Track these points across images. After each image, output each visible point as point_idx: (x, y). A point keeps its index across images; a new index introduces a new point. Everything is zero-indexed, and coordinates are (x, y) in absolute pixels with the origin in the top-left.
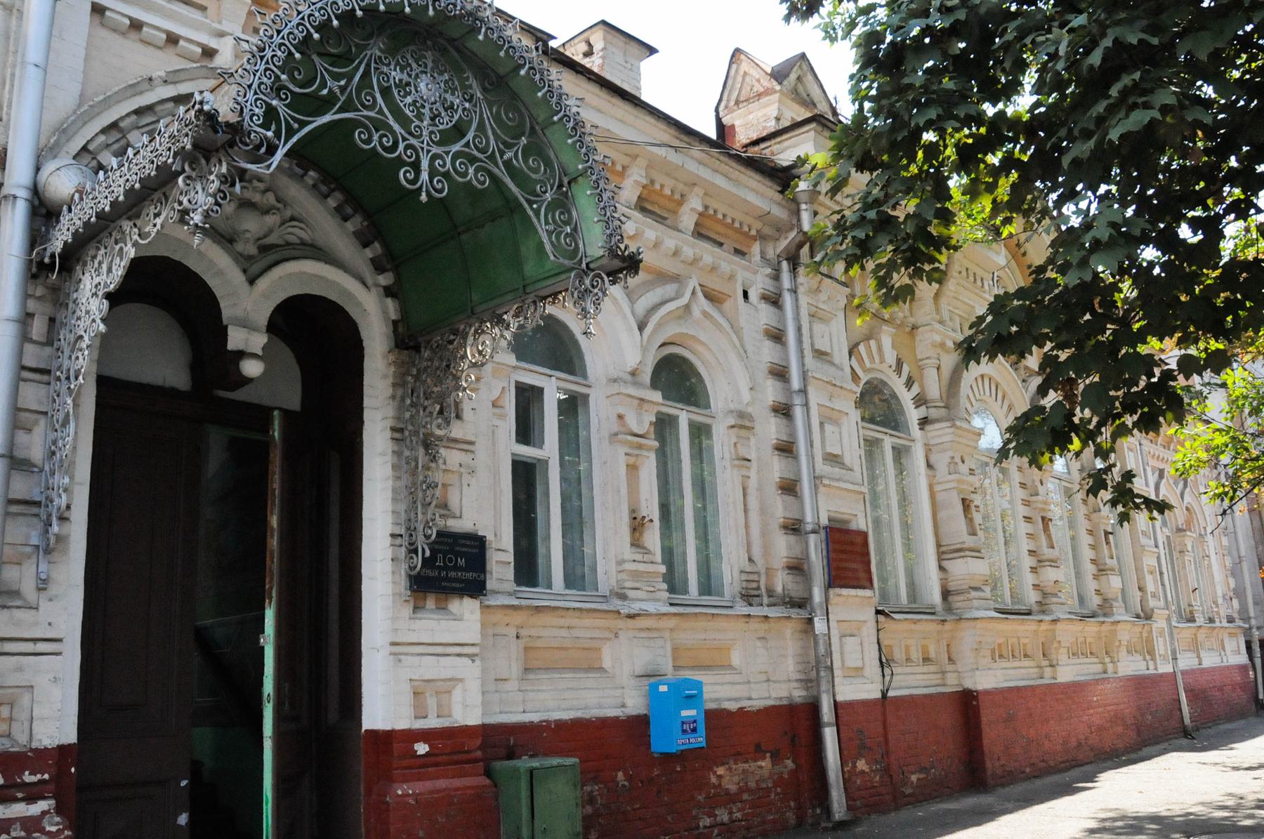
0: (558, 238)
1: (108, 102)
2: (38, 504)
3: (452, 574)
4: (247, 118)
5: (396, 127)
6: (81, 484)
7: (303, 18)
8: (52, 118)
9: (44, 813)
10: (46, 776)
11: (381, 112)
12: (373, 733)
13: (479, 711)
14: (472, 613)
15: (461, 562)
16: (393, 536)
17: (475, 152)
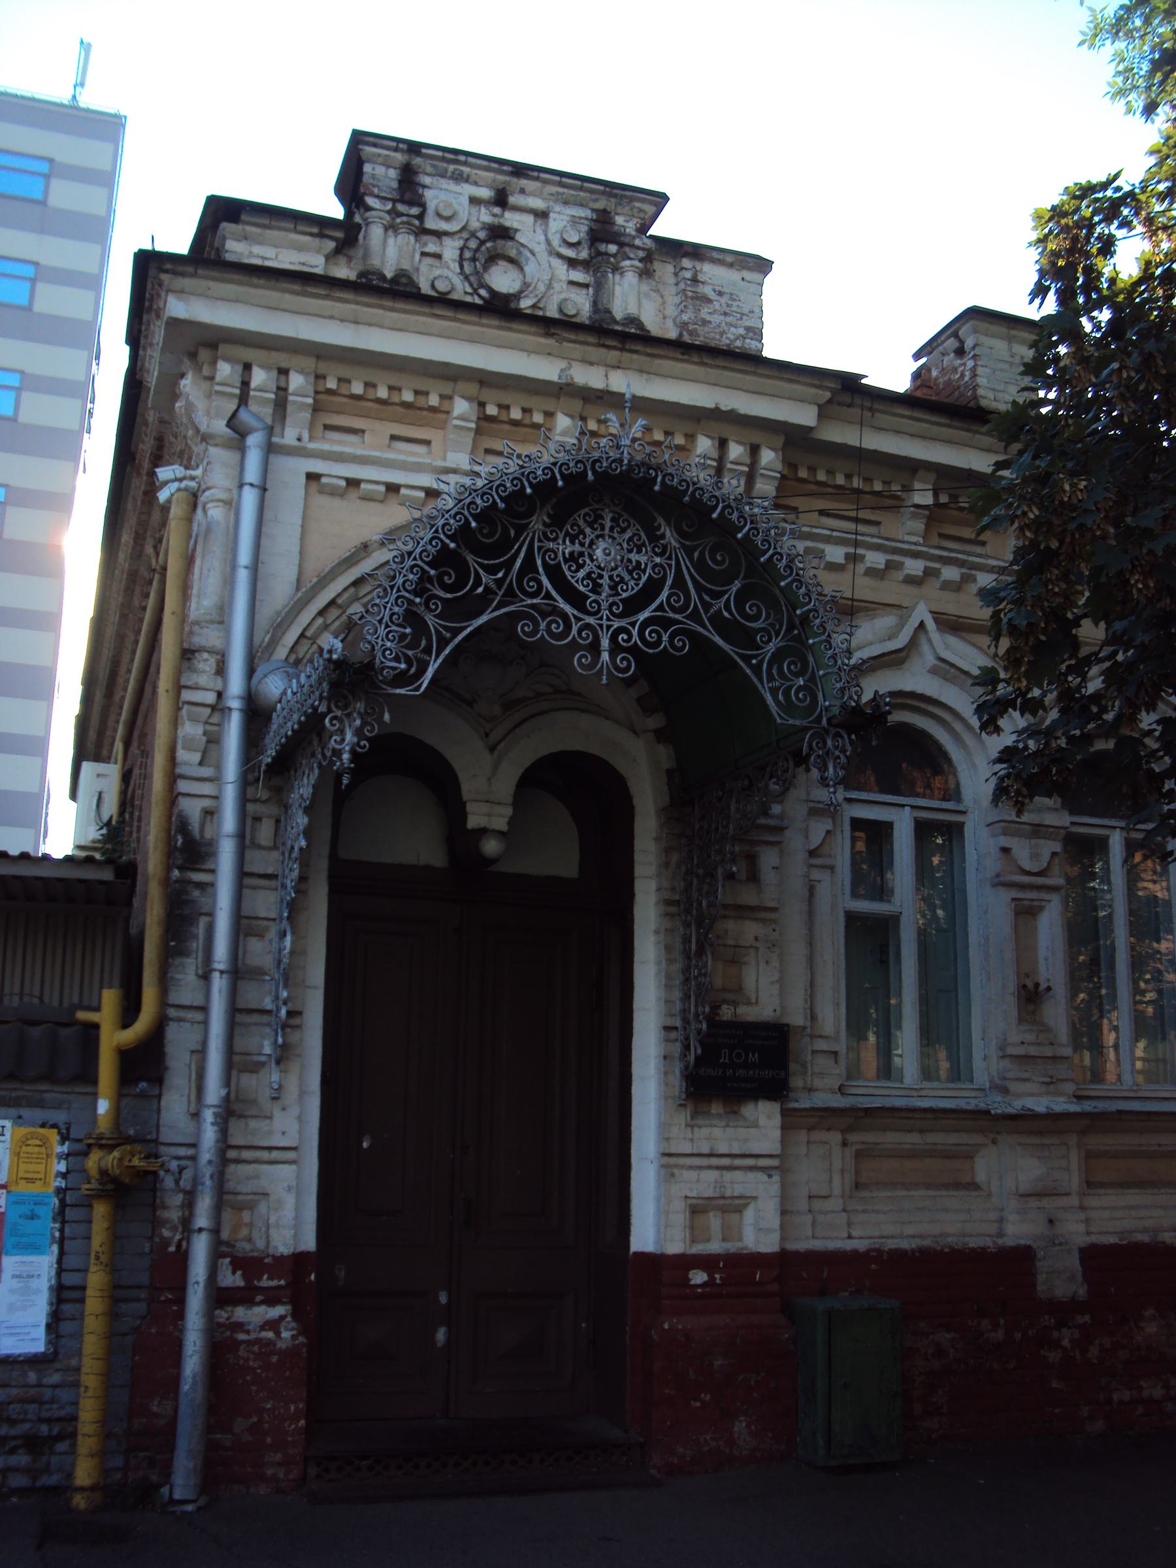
1: (324, 581)
2: (269, 1012)
3: (741, 1072)
4: (379, 655)
5: (567, 608)
6: (315, 988)
7: (491, 488)
9: (282, 1318)
10: (282, 1282)
11: (548, 596)
12: (642, 1256)
14: (769, 1117)
15: (754, 1058)
16: (667, 1029)
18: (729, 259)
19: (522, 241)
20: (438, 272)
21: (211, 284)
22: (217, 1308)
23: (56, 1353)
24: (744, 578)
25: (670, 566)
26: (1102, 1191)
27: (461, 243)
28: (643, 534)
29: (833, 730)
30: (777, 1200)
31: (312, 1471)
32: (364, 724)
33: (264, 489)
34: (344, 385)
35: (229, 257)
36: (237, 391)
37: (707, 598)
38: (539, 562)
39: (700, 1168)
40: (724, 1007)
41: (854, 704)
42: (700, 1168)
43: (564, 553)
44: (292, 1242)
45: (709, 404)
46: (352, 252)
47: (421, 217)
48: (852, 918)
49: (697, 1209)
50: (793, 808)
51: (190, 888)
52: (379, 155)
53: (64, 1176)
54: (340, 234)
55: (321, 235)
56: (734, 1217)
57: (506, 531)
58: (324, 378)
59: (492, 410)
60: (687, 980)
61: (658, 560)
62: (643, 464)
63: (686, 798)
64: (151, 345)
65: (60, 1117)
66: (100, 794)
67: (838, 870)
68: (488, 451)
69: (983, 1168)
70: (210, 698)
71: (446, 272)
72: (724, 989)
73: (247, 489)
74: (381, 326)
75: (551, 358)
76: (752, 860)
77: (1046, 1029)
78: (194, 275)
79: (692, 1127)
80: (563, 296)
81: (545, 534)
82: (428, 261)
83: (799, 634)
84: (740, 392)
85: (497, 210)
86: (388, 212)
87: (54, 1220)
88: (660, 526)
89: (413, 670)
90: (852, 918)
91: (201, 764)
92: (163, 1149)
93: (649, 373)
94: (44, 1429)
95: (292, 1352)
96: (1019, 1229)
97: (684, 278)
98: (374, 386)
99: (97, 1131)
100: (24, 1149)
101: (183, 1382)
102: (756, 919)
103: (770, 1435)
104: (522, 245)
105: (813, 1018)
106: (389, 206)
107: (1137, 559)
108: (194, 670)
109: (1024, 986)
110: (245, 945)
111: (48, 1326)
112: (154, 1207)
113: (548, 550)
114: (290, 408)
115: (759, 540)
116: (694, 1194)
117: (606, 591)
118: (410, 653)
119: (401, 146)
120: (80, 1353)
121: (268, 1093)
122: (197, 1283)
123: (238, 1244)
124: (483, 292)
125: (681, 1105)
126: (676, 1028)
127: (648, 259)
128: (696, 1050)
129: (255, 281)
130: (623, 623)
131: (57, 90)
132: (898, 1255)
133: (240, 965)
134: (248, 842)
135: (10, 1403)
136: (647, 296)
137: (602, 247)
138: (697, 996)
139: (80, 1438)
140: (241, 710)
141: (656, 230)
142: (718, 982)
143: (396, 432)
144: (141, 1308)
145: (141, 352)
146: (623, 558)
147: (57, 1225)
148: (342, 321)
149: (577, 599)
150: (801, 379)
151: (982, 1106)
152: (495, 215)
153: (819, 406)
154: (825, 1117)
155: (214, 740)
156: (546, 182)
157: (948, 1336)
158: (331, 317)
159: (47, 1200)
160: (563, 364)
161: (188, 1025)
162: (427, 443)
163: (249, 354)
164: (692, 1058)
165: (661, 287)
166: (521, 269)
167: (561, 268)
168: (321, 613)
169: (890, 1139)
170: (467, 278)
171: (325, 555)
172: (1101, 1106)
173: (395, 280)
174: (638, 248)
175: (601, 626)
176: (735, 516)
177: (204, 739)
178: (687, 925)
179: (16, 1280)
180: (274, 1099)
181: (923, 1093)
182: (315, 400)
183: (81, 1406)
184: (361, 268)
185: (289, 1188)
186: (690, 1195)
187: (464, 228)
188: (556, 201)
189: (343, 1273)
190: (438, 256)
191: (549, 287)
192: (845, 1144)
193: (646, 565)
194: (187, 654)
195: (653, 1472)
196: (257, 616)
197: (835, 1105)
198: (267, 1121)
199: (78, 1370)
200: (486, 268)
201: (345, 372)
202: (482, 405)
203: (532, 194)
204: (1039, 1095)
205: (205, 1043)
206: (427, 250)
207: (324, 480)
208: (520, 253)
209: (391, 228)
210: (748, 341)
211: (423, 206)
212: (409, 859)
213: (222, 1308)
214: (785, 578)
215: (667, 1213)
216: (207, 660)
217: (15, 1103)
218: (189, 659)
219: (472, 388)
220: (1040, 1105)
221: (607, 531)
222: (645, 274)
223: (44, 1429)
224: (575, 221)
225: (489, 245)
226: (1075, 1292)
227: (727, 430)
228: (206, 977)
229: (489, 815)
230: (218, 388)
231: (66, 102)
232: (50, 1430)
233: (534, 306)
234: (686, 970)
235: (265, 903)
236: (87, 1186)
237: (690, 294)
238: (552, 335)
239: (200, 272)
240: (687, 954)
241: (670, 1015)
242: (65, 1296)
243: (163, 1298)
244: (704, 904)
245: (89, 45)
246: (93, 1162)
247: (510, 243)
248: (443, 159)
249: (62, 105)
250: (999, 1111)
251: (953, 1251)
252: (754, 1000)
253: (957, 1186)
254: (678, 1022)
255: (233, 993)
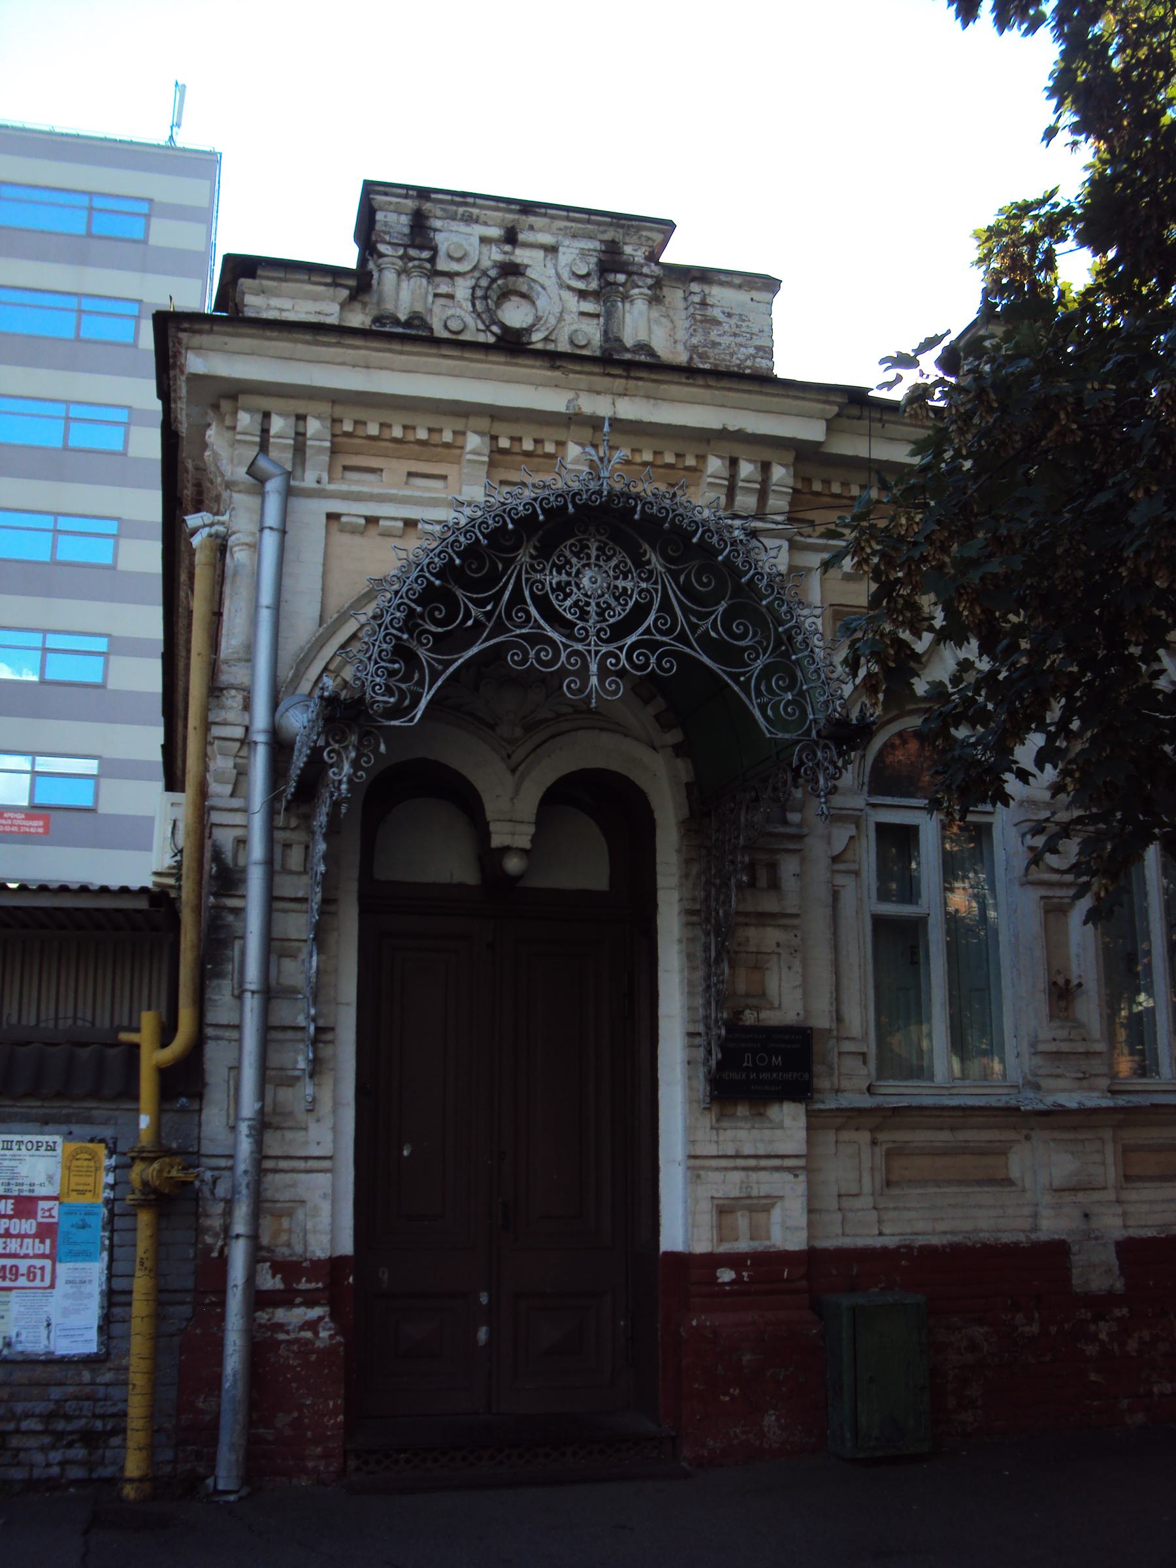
0: (775, 708)
1: (343, 618)
3: (764, 1076)
4: (369, 691)
6: (348, 1004)
7: (473, 526)
8: (336, 603)
9: (320, 1319)
10: (320, 1285)
12: (672, 1256)
13: (804, 1235)
14: (794, 1119)
15: (777, 1061)
16: (691, 1035)
17: (658, 637)
18: (737, 281)
19: (533, 276)
20: (450, 312)
21: (227, 339)
22: (256, 1311)
23: (108, 1353)
24: (730, 599)
25: (656, 590)
26: (1139, 1184)
27: (472, 282)
28: (628, 561)
29: (822, 742)
30: (804, 1199)
31: (352, 1464)
32: (359, 756)
33: (283, 532)
34: (360, 427)
35: (249, 313)
36: (258, 439)
37: (694, 620)
38: (527, 594)
39: (726, 1169)
40: (747, 1012)
41: (837, 715)
42: (726, 1169)
43: (551, 583)
44: (328, 1246)
45: (716, 425)
46: (366, 298)
47: (432, 260)
48: (880, 924)
49: (724, 1210)
50: (808, 813)
51: (224, 914)
52: (391, 203)
53: (112, 1187)
54: (352, 283)
55: (336, 285)
56: (762, 1217)
57: (494, 566)
58: (341, 421)
59: (504, 443)
60: (708, 987)
61: (644, 585)
62: (623, 494)
63: (705, 808)
64: (180, 398)
65: (108, 1132)
66: (175, 822)
67: (864, 875)
68: (502, 483)
69: (1017, 1164)
70: (239, 732)
71: (458, 312)
72: (748, 995)
73: (267, 532)
74: (392, 370)
75: (558, 390)
76: (773, 867)
77: (1079, 1025)
78: (211, 332)
79: (717, 1129)
80: (574, 327)
81: (532, 566)
82: (441, 301)
83: (787, 650)
84: (747, 412)
85: (508, 248)
86: (401, 258)
87: (104, 1229)
88: (645, 553)
89: (407, 702)
90: (880, 924)
91: (232, 795)
92: (205, 1161)
93: (655, 399)
94: (99, 1424)
95: (330, 1351)
96: (1053, 1225)
97: (693, 303)
98: (390, 426)
99: (140, 1145)
100: (75, 1163)
101: (224, 1379)
102: (774, 926)
103: (800, 1428)
104: (533, 280)
105: (839, 1019)
106: (401, 252)
107: (964, 588)
108: (223, 707)
109: (1055, 983)
110: (279, 966)
111: (100, 1328)
112: (197, 1215)
113: (536, 581)
114: (309, 452)
115: (739, 561)
116: (720, 1195)
117: (594, 617)
118: (404, 686)
119: (411, 192)
120: (127, 1352)
121: (303, 1105)
122: (236, 1286)
123: (278, 1250)
124: (495, 329)
125: (705, 1109)
126: (699, 1034)
127: (658, 284)
128: (717, 1054)
129: (268, 333)
130: (611, 647)
131: (154, 133)
132: (929, 1252)
133: (273, 982)
134: (277, 867)
135: (66, 1401)
136: (657, 322)
137: (611, 277)
138: (717, 1003)
139: (129, 1432)
140: (266, 743)
141: (666, 257)
142: (742, 987)
143: (413, 469)
144: (186, 1310)
145: (173, 406)
146: (609, 585)
147: (107, 1234)
148: (354, 366)
149: (640, 611)
150: (807, 395)
151: (1013, 1103)
152: (505, 253)
153: (827, 421)
154: (853, 1117)
155: (242, 772)
156: (553, 217)
157: (982, 1330)
158: (343, 364)
159: (96, 1210)
160: (571, 395)
161: (225, 1043)
162: (444, 478)
163: (266, 403)
164: (713, 1063)
165: (671, 313)
166: (533, 303)
167: (571, 300)
168: (343, 647)
169: (921, 1137)
170: (479, 315)
171: (346, 590)
172: (1136, 1100)
173: (408, 324)
174: (647, 276)
175: (589, 651)
176: (715, 539)
177: (235, 771)
178: (707, 934)
179: (68, 1286)
180: (309, 1111)
181: (954, 1091)
182: (332, 443)
183: (130, 1403)
184: (375, 312)
185: (325, 1196)
186: (716, 1195)
187: (475, 268)
188: (565, 235)
189: (386, 1276)
190: (451, 297)
191: (560, 319)
192: (874, 1143)
193: (633, 590)
194: (215, 690)
195: (685, 1464)
196: (280, 652)
197: (861, 1105)
198: (302, 1133)
199: (126, 1369)
200: (498, 304)
201: (360, 414)
202: (494, 438)
203: (541, 230)
204: (1071, 1091)
205: (240, 1059)
206: (439, 291)
207: (344, 519)
208: (531, 288)
209: (403, 272)
210: (758, 360)
211: (435, 250)
212: (444, 878)
213: (262, 1310)
214: (767, 597)
215: (694, 1213)
216: (234, 697)
217: (67, 1120)
218: (218, 697)
219: (484, 423)
220: (1071, 1101)
221: (593, 560)
222: (655, 300)
223: (99, 1424)
224: (583, 253)
225: (500, 282)
226: (1112, 1286)
227: (736, 449)
228: (240, 997)
229: (513, 834)
230: (239, 437)
231: (162, 143)
232: (105, 1425)
233: (546, 339)
234: (708, 977)
235: (297, 925)
236: (131, 1197)
237: (699, 317)
238: (558, 368)
239: (215, 328)
240: (707, 961)
241: (693, 1021)
242: (115, 1299)
243: (207, 1301)
244: (721, 913)
245: (184, 86)
246: (137, 1173)
247: (521, 279)
248: (452, 203)
249: (159, 146)
250: (1029, 1108)
251: (985, 1246)
252: (776, 1004)
253: (991, 1182)
254: (701, 1028)
255: (265, 1012)
